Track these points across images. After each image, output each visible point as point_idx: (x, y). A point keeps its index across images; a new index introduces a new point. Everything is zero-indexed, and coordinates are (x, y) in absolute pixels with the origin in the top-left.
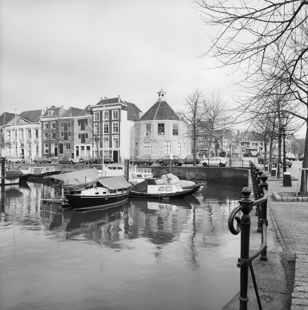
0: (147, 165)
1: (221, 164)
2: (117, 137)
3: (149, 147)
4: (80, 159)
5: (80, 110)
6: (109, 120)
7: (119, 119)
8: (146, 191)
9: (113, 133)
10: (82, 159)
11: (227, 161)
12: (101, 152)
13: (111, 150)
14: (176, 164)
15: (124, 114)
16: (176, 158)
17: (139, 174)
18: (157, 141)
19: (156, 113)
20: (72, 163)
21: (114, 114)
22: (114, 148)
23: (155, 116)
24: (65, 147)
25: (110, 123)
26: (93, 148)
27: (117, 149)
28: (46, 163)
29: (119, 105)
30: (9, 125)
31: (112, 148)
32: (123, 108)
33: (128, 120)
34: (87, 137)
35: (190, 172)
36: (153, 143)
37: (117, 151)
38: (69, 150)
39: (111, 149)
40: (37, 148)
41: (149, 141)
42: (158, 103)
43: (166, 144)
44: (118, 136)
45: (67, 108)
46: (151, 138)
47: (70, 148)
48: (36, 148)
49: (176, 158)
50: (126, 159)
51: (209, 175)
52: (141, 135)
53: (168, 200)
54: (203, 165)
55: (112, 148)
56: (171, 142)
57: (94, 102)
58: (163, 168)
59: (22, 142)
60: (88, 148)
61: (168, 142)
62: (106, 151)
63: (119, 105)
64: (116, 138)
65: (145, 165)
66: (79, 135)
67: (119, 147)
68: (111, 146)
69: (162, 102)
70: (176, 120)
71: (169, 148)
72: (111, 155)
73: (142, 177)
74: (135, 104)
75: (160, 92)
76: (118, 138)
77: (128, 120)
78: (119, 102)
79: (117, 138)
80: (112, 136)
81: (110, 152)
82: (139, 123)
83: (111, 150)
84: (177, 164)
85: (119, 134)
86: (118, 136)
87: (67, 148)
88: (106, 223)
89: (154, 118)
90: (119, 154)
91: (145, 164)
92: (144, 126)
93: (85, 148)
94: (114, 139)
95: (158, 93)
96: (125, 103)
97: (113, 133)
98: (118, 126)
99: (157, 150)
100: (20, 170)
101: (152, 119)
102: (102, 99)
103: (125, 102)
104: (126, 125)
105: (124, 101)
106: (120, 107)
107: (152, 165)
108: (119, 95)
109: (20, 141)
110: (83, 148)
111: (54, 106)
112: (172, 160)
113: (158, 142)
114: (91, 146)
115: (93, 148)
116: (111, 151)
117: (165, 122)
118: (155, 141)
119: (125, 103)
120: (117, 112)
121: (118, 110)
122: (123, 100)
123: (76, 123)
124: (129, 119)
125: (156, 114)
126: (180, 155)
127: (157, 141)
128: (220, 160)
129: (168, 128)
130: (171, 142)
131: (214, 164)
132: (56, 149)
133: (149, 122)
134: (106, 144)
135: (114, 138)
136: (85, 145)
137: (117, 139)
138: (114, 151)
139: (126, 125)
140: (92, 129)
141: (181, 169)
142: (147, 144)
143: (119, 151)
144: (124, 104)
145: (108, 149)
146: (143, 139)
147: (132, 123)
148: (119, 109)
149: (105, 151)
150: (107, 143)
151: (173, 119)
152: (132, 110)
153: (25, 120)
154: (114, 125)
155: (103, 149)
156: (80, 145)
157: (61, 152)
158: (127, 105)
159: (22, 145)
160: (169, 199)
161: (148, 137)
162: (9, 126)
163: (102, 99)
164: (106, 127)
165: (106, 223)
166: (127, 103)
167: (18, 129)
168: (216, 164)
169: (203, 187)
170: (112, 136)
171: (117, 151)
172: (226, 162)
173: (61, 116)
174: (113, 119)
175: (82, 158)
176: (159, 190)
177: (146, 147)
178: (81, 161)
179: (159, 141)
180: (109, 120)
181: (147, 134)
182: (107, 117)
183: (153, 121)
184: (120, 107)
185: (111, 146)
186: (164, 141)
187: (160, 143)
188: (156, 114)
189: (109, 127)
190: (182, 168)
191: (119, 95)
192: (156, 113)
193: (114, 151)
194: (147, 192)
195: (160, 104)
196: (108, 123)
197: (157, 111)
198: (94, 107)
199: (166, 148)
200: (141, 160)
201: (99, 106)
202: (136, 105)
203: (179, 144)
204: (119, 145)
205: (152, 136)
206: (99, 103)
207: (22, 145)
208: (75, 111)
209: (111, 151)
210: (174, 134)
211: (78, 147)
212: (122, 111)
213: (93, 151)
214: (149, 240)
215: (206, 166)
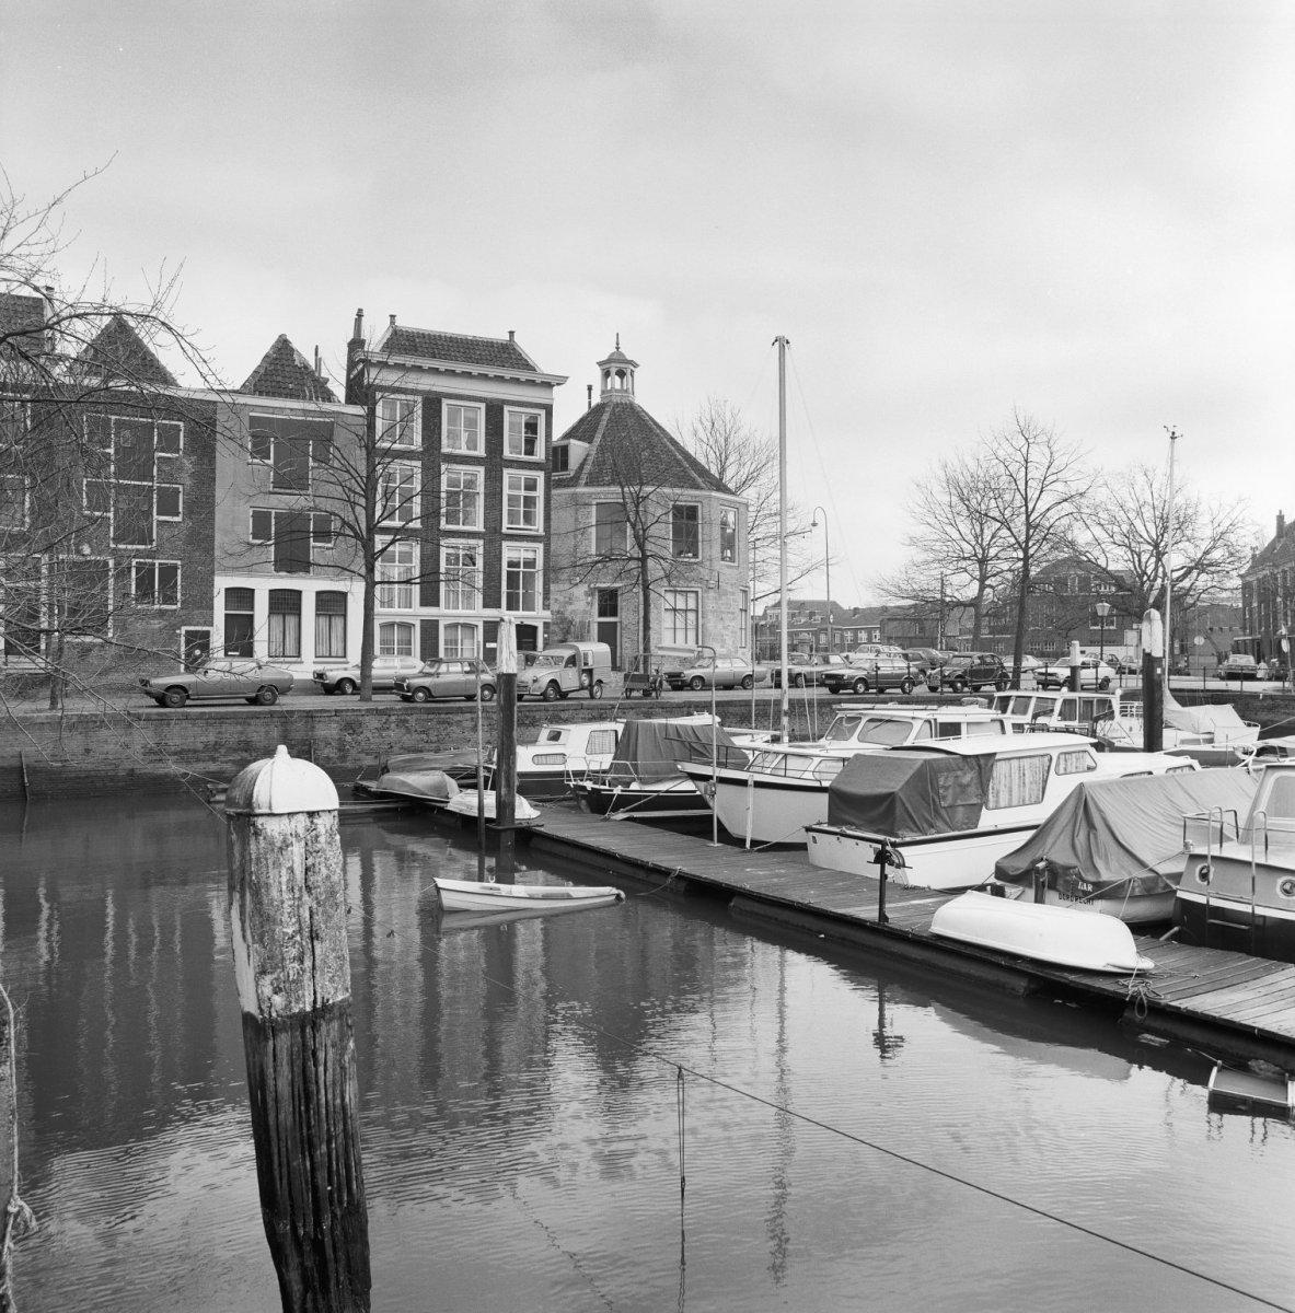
13: (437, 621)
25: (424, 468)
38: (162, 613)
60: (331, 604)
62: (455, 626)
66: (261, 519)
79: (530, 555)
80: (504, 544)
81: (485, 632)
83: (437, 621)
88: (236, 906)
93: (308, 605)
95: (600, 364)
100: (365, 783)
110: (285, 603)
130: (697, 592)
136: (309, 587)
140: (1163, 468)
156: (263, 586)
165: (236, 906)
170: (504, 544)
171: (535, 628)
183: (710, 497)
196: (481, 471)
214: (1098, 852)
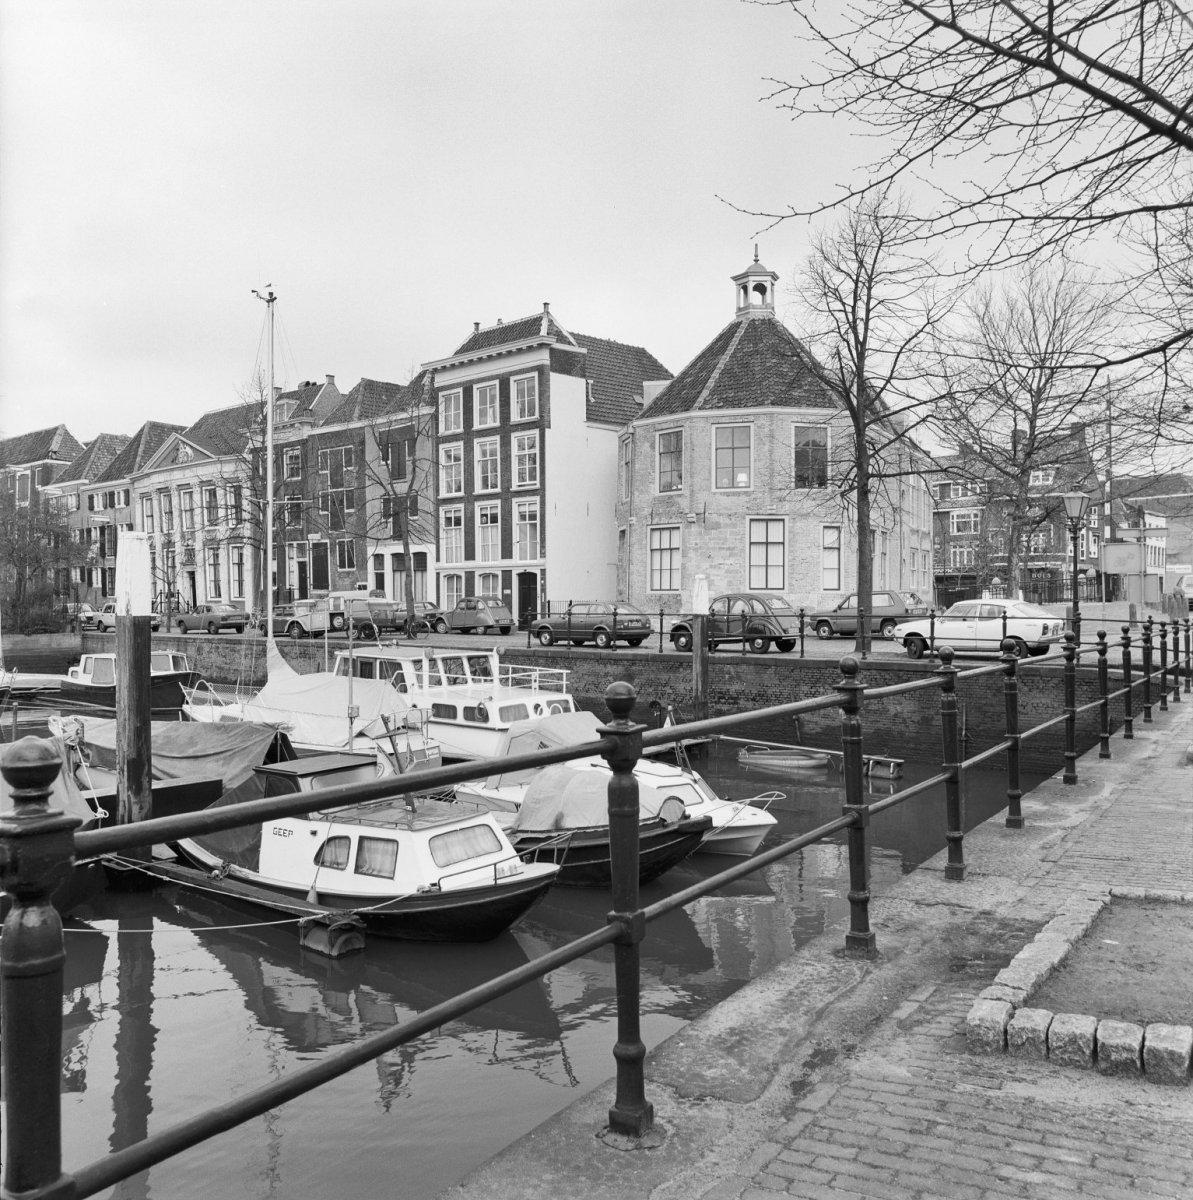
0: (607, 646)
1: (1013, 646)
2: (531, 504)
3: (674, 552)
4: (332, 616)
5: (391, 389)
6: (498, 424)
7: (541, 416)
8: (251, 858)
9: (514, 488)
10: (342, 614)
11: (1051, 624)
12: (467, 580)
14: (754, 640)
15: (568, 393)
16: (756, 604)
17: (475, 705)
18: (714, 518)
19: (716, 374)
20: (296, 631)
21: (520, 393)
22: (518, 563)
23: (705, 393)
24: (332, 561)
26: (438, 560)
27: (532, 565)
28: (217, 633)
29: (541, 346)
30: (146, 471)
31: (511, 557)
32: (565, 363)
33: (590, 424)
34: (415, 511)
35: (822, 690)
36: (694, 529)
37: (535, 575)
38: (348, 573)
39: (507, 562)
40: (240, 564)
41: (673, 520)
42: (733, 329)
43: (758, 532)
44: (537, 499)
45: (345, 386)
46: (684, 503)
47: (351, 565)
48: (236, 567)
49: (759, 608)
50: (124, 614)
51: (932, 712)
52: (636, 493)
53: (329, 957)
54: (906, 650)
55: (511, 557)
56: (783, 520)
57: (445, 348)
58: (681, 664)
59: (190, 542)
61: (767, 521)
63: (541, 346)
64: (526, 509)
65: (597, 646)
67: (543, 555)
68: (507, 553)
69: (754, 320)
70: (816, 406)
71: (775, 554)
72: (507, 592)
73: (486, 718)
74: (650, 350)
75: (745, 275)
76: (537, 508)
77: (589, 419)
78: (544, 331)
79: (533, 508)
82: (631, 430)
84: (760, 641)
85: (541, 492)
86: (537, 499)
87: (342, 565)
89: (701, 399)
90: (543, 590)
91: (601, 640)
92: (653, 447)
94: (523, 517)
95: (735, 278)
96: (572, 340)
97: (514, 488)
98: (537, 450)
99: (711, 566)
101: (687, 406)
102: (477, 329)
103: (576, 336)
104: (577, 447)
105: (572, 334)
106: (544, 358)
107: (644, 643)
108: (546, 304)
109: (183, 536)
111: (311, 381)
112: (703, 616)
113: (717, 526)
114: (429, 549)
115: (438, 560)
116: (507, 574)
117: (752, 418)
118: (702, 518)
119: (572, 340)
120: (530, 384)
121: (535, 374)
122: (567, 326)
123: (372, 451)
124: (594, 414)
125: (711, 383)
126: (839, 589)
127: (713, 518)
128: (1005, 618)
129: (771, 452)
130: (783, 520)
131: (972, 644)
132: (302, 566)
133: (673, 421)
134: (488, 538)
135: (522, 509)
137: (533, 517)
138: (520, 575)
139: (577, 447)
141: (771, 671)
142: (666, 534)
143: (543, 572)
144: (570, 343)
145: (497, 564)
146: (647, 511)
147: (605, 440)
148: (540, 369)
149: (485, 576)
150: (495, 533)
151: (798, 403)
152: (616, 377)
153: (198, 447)
154: (521, 447)
155: (479, 564)
157: (321, 582)
158: (584, 351)
159: (190, 553)
160: (335, 953)
161: (671, 497)
162: (148, 475)
163: (477, 329)
164: (488, 458)
166: (581, 339)
167: (194, 481)
168: (980, 644)
169: (766, 818)
170: (515, 500)
171: (535, 575)
172: (1045, 628)
173: (321, 422)
174: (515, 418)
175: (342, 607)
176: (319, 859)
177: (661, 550)
178: (338, 622)
179: (723, 520)
180: (498, 424)
181: (667, 487)
182: (490, 412)
184: (544, 358)
185: (507, 553)
186: (748, 518)
187: (729, 530)
188: (711, 383)
189: (498, 458)
190: (802, 665)
191: (546, 304)
192: (716, 374)
193: (520, 575)
194: (255, 868)
195: (741, 332)
197: (721, 366)
198: (439, 367)
199: (758, 553)
200: (574, 620)
201: (465, 358)
202: (636, 345)
203: (831, 531)
204: (543, 546)
205: (686, 492)
206: (465, 349)
207: (190, 553)
208: (376, 396)
209: (507, 574)
210: (802, 481)
211: (379, 558)
212: (557, 380)
213: (438, 574)
215: (921, 656)
